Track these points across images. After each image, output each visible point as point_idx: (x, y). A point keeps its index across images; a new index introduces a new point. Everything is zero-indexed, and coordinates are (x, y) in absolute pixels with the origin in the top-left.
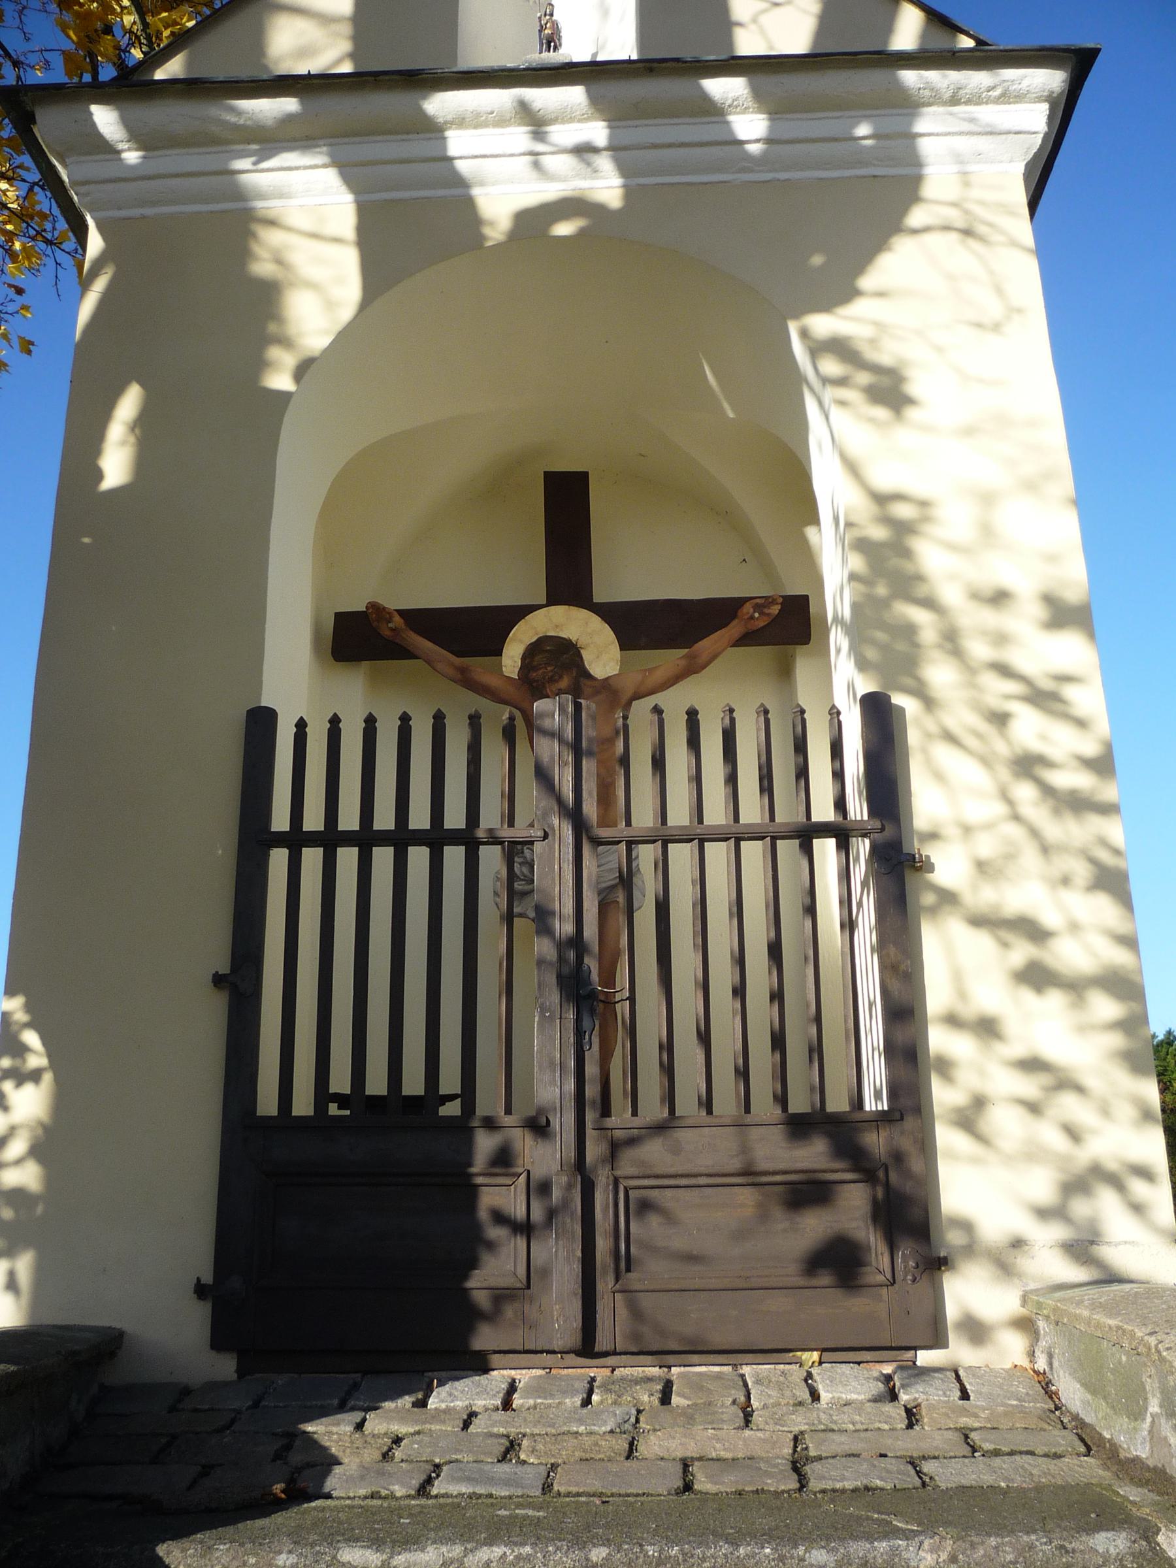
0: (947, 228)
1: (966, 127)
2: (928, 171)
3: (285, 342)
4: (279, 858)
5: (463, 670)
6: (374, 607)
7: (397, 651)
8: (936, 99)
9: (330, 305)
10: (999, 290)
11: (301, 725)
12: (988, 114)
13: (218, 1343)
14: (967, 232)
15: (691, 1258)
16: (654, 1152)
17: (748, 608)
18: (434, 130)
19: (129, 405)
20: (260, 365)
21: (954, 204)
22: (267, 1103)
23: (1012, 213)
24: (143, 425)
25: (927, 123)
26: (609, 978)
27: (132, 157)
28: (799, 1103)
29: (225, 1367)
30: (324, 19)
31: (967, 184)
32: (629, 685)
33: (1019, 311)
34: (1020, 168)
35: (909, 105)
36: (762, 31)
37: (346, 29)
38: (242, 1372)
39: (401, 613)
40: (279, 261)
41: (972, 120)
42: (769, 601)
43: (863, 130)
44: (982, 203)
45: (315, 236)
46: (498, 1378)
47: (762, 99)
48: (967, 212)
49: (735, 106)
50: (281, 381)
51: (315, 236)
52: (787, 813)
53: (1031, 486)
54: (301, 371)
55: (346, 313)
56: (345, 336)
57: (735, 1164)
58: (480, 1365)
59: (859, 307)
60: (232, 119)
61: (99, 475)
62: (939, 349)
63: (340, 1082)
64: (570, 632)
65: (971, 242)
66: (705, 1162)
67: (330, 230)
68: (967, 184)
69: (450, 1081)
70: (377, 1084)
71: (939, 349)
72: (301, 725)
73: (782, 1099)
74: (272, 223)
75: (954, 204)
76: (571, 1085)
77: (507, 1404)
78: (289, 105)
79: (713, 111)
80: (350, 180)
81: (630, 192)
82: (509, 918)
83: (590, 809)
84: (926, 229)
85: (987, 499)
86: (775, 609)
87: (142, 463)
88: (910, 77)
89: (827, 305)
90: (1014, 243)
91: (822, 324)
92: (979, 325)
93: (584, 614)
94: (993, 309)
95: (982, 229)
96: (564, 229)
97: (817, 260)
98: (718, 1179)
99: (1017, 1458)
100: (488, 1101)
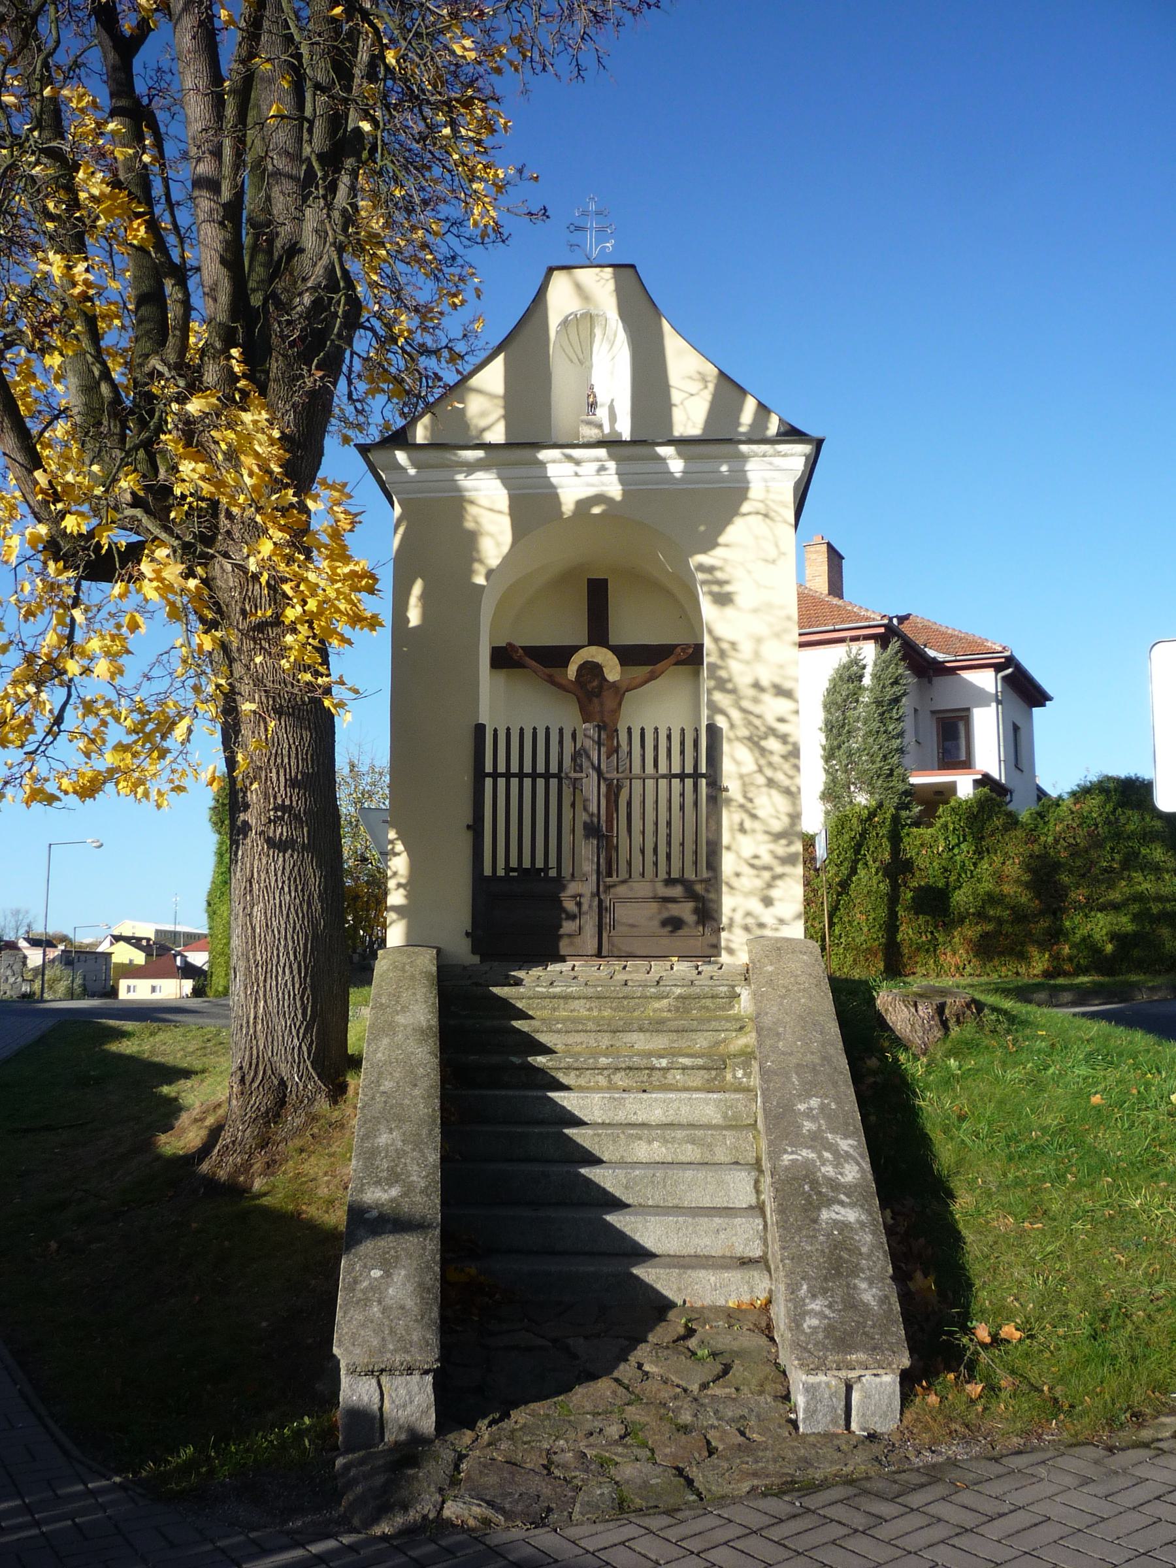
0: (758, 513)
1: (769, 467)
2: (751, 485)
3: (481, 561)
4: (489, 782)
5: (550, 676)
6: (510, 644)
7: (518, 665)
8: (756, 455)
9: (498, 545)
10: (777, 546)
11: (495, 730)
12: (777, 461)
13: (474, 952)
14: (766, 516)
15: (632, 926)
16: (621, 890)
17: (678, 650)
18: (542, 464)
19: (417, 589)
20: (470, 572)
21: (762, 501)
22: (488, 871)
23: (784, 505)
24: (424, 597)
25: (751, 466)
26: (610, 828)
27: (412, 471)
28: (675, 874)
29: (476, 959)
30: (492, 396)
31: (768, 491)
32: (624, 686)
33: (784, 554)
34: (792, 484)
35: (744, 458)
36: (685, 408)
37: (501, 402)
38: (481, 961)
39: (523, 648)
40: (477, 522)
41: (771, 464)
42: (688, 646)
43: (724, 468)
44: (773, 501)
45: (491, 510)
46: (570, 964)
47: (680, 455)
48: (767, 505)
49: (670, 457)
50: (480, 580)
51: (491, 510)
52: (676, 770)
53: (777, 635)
54: (489, 574)
55: (506, 549)
56: (506, 559)
57: (651, 895)
58: (562, 959)
59: (718, 552)
60: (454, 458)
61: (408, 621)
62: (749, 572)
63: (514, 863)
64: (599, 659)
65: (767, 520)
66: (641, 894)
67: (497, 507)
68: (768, 491)
69: (553, 862)
70: (527, 864)
71: (749, 572)
72: (495, 730)
73: (669, 873)
74: (472, 502)
75: (762, 501)
76: (595, 867)
77: (573, 969)
78: (480, 454)
79: (662, 459)
80: (506, 481)
81: (625, 493)
82: (573, 805)
83: (603, 766)
84: (749, 514)
85: (759, 640)
86: (691, 651)
87: (425, 615)
88: (744, 448)
89: (705, 550)
90: (785, 522)
91: (701, 558)
92: (767, 561)
93: (605, 650)
94: (772, 553)
95: (772, 514)
96: (596, 510)
97: (702, 528)
98: (645, 900)
99: (595, 877)
100: (566, 872)
